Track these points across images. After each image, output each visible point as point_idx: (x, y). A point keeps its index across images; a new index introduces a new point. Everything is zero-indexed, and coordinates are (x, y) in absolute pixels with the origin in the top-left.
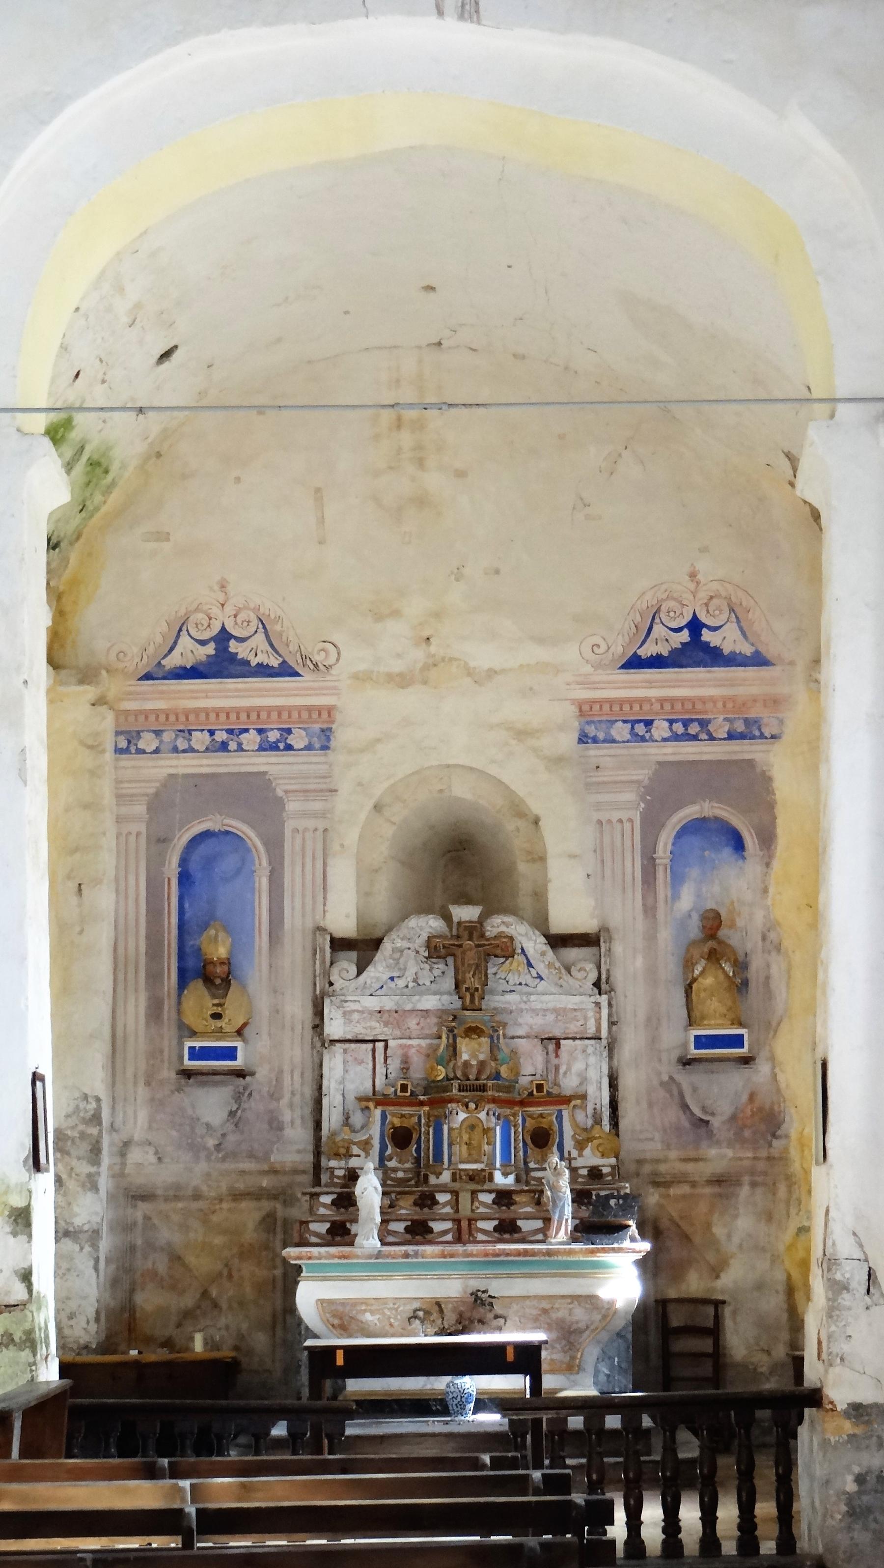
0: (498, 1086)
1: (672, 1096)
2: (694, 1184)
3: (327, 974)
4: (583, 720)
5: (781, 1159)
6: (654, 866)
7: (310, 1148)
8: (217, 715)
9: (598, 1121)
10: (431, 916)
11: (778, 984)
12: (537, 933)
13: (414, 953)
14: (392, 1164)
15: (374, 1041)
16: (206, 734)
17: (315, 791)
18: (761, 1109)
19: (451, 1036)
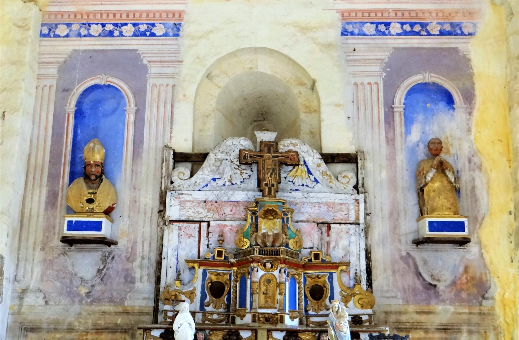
0: (288, 252)
1: (409, 266)
2: (426, 330)
3: (169, 176)
4: (345, 21)
5: (489, 314)
6: (393, 112)
7: (152, 296)
8: (108, 15)
9: (358, 281)
10: (243, 138)
11: (481, 193)
12: (315, 151)
13: (230, 162)
14: (209, 309)
15: (200, 222)
16: (100, 26)
17: (168, 61)
18: (473, 278)
19: (254, 217)
